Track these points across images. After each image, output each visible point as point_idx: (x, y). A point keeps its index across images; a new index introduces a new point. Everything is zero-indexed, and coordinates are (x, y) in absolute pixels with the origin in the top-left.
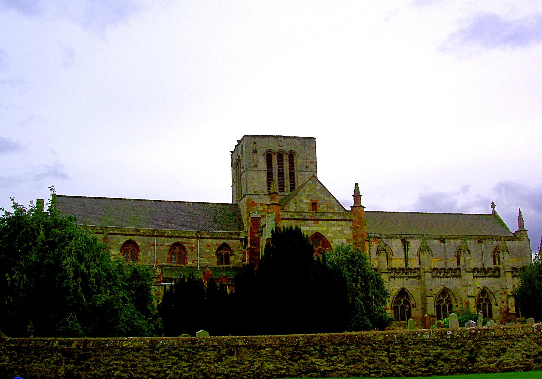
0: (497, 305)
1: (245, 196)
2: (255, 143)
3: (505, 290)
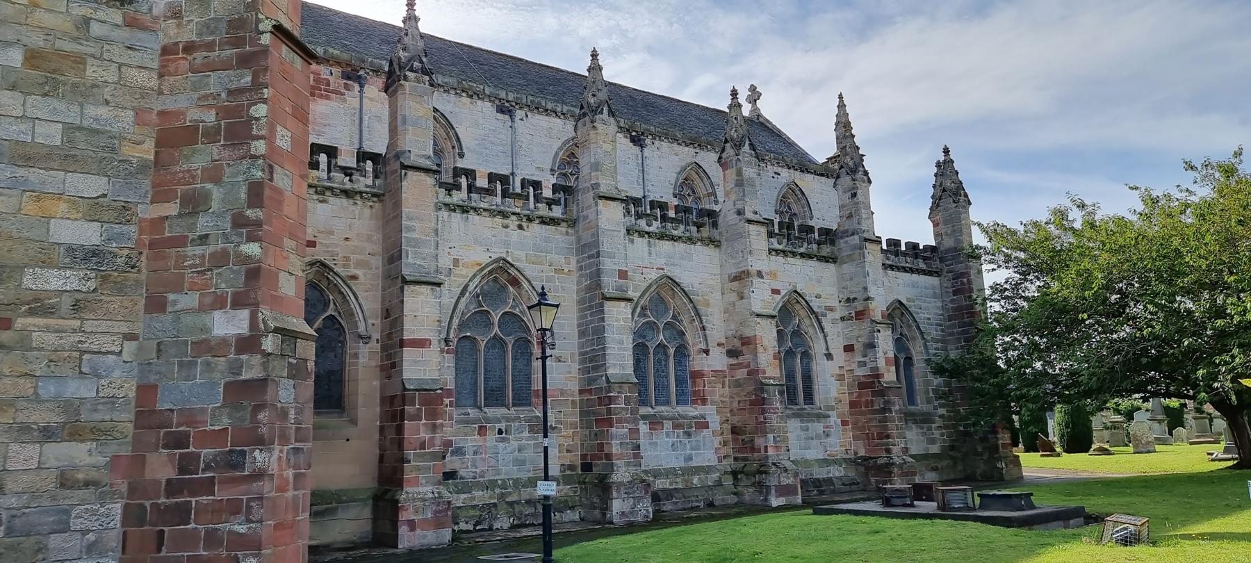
0: (829, 356)
3: (859, 306)
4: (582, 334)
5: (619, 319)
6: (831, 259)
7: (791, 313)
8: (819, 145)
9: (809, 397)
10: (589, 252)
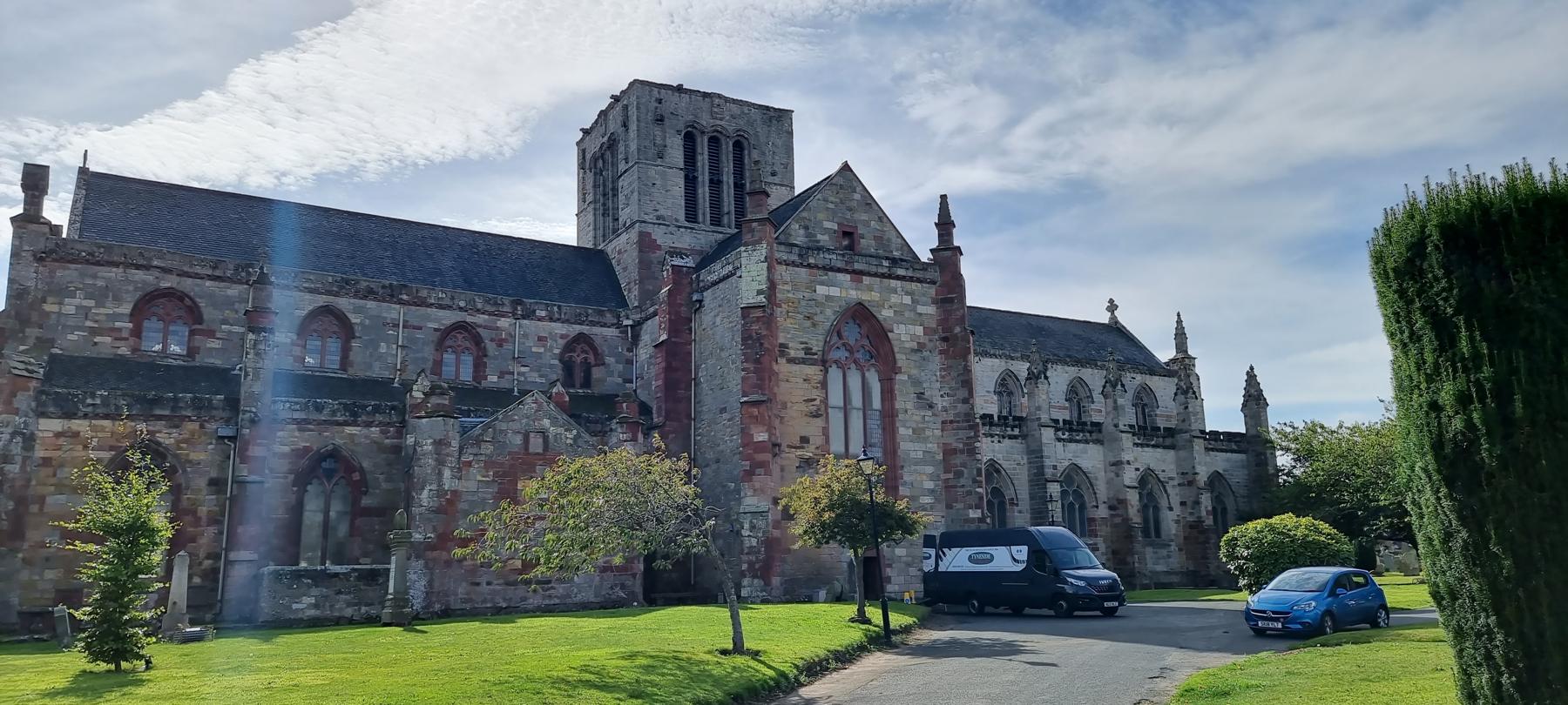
0: (1171, 509)
1: (633, 224)
2: (660, 101)
4: (1032, 498)
5: (1054, 489)
6: (1172, 447)
7: (1147, 481)
8: (1165, 353)
9: (1158, 534)
10: (1035, 455)
